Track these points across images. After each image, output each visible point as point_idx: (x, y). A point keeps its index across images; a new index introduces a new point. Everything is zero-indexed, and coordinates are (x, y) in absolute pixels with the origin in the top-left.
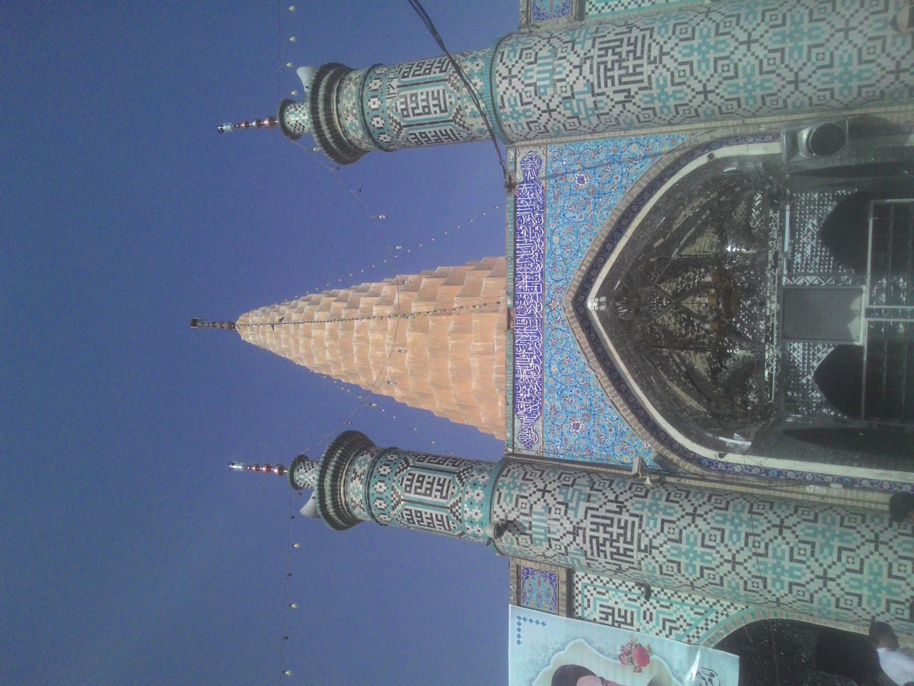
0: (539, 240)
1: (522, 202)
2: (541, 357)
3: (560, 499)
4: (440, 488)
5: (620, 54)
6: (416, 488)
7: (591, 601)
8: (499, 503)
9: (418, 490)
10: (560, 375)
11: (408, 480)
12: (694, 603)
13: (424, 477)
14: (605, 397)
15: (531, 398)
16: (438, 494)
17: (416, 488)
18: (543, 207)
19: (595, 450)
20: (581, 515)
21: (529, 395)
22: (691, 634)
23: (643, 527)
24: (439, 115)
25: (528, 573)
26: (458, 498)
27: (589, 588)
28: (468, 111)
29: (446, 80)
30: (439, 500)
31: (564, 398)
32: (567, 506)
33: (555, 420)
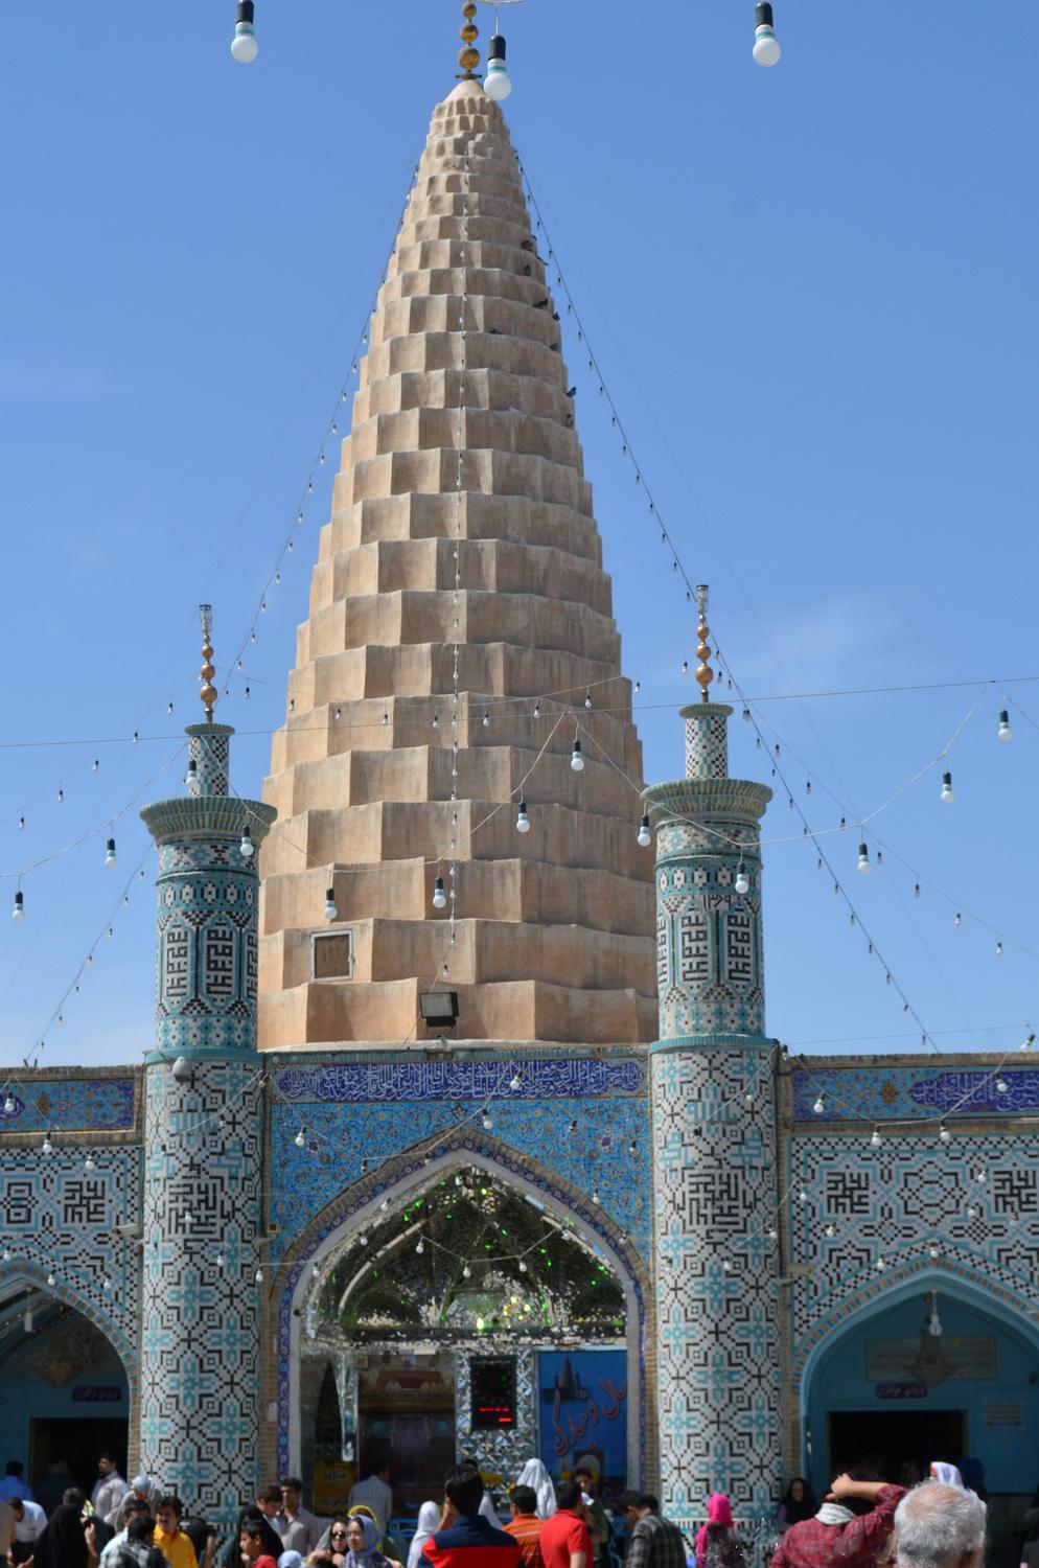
0: (537, 1091)
1: (584, 1066)
2: (394, 1099)
3: (228, 1145)
4: (220, 981)
5: (721, 1198)
6: (216, 947)
7: (107, 1171)
8: (213, 1067)
9: (213, 950)
10: (374, 1123)
11: (224, 932)
12: (128, 1290)
13: (230, 954)
14: (352, 1181)
15: (343, 1086)
16: (212, 980)
17: (216, 947)
18: (577, 1096)
19: (288, 1169)
20: (215, 1172)
21: (346, 1083)
22: (92, 1288)
23: (210, 1244)
24: (727, 967)
25: (127, 1089)
26: (210, 1008)
27: (122, 1167)
28: (726, 1007)
29: (718, 981)
30: (205, 981)
31: (347, 1130)
32: (222, 1154)
33: (319, 1119)
